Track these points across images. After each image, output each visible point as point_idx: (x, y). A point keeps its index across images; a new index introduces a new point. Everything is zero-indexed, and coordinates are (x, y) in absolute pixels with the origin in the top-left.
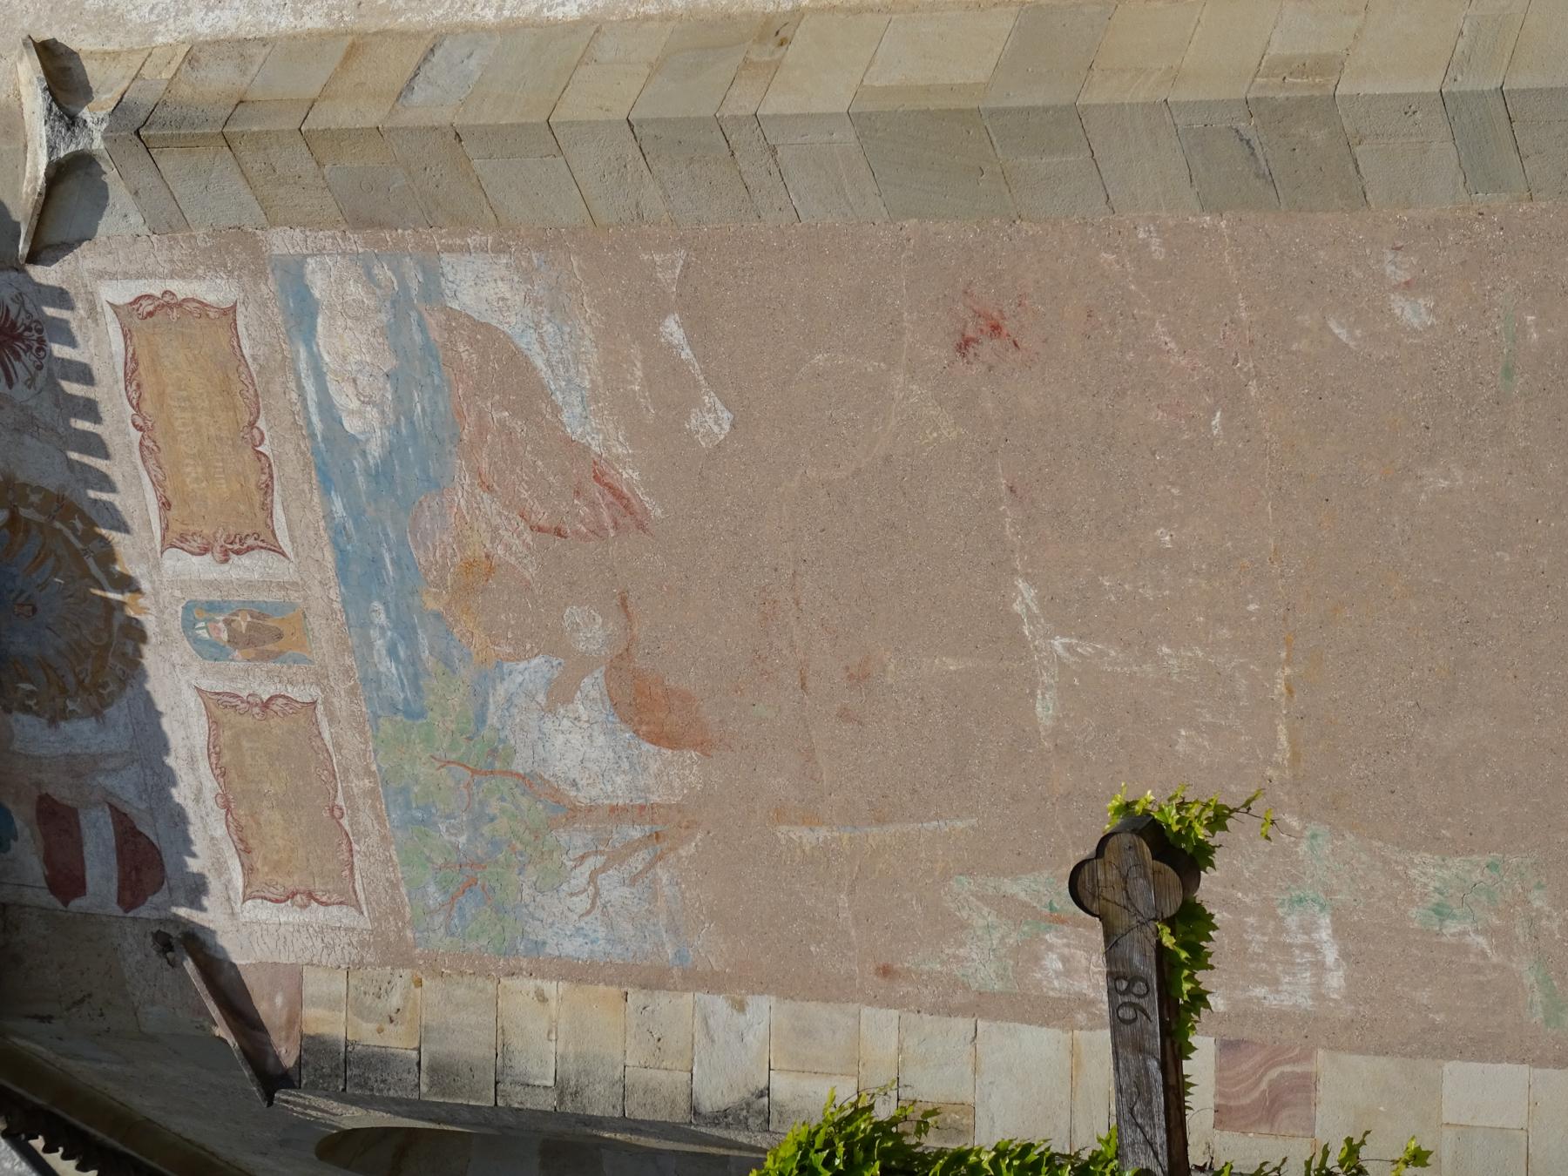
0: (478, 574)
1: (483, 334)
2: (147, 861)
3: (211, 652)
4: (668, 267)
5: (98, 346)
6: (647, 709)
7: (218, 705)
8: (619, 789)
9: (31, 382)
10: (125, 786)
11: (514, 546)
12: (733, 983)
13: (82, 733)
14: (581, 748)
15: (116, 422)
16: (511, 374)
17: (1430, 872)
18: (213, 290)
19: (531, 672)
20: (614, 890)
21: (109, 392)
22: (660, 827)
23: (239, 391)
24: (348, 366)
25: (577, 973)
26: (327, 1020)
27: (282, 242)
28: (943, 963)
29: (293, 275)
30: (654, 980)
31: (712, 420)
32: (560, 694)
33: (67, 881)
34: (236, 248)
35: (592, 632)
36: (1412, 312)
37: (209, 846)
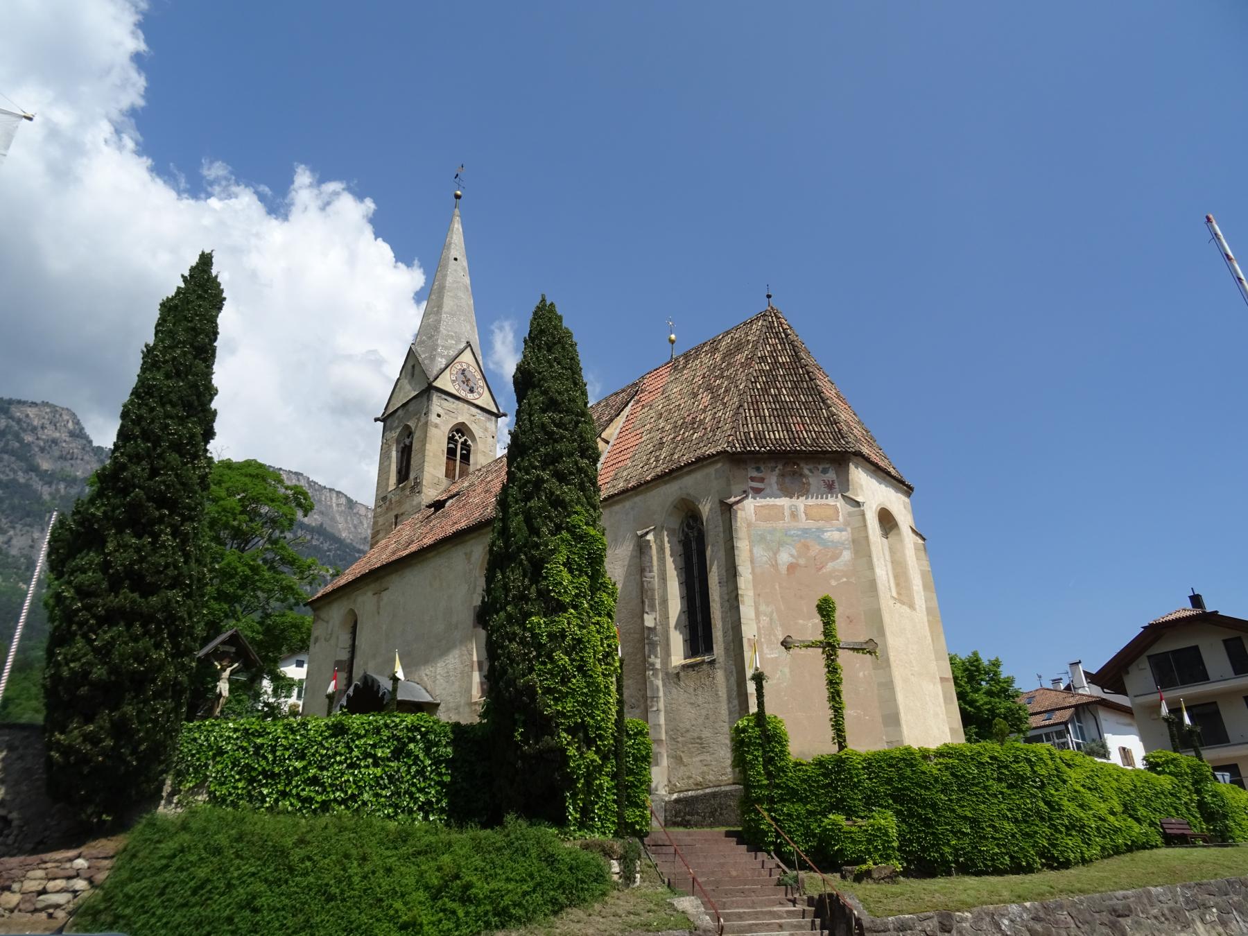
0: (807, 547)
1: (841, 554)
2: (758, 491)
3: (790, 508)
4: (853, 580)
5: (831, 501)
6: (792, 568)
7: (782, 507)
8: (780, 562)
9: (1057, 790)
10: (768, 491)
11: (812, 553)
12: (753, 573)
13: (775, 487)
14: (784, 558)
15: (819, 501)
16: (835, 557)
17: (787, 670)
18: (841, 518)
19: (794, 552)
20: (765, 559)
21: (824, 501)
22: (775, 566)
23: (828, 519)
24: (833, 535)
25: (751, 551)
26: (740, 514)
27: (849, 529)
28: (467, 914)
29: (845, 530)
30: (752, 562)
31: (834, 583)
32: (792, 556)
33: (753, 479)
34: (847, 524)
35: (802, 561)
36: (861, 674)
37: (761, 502)
